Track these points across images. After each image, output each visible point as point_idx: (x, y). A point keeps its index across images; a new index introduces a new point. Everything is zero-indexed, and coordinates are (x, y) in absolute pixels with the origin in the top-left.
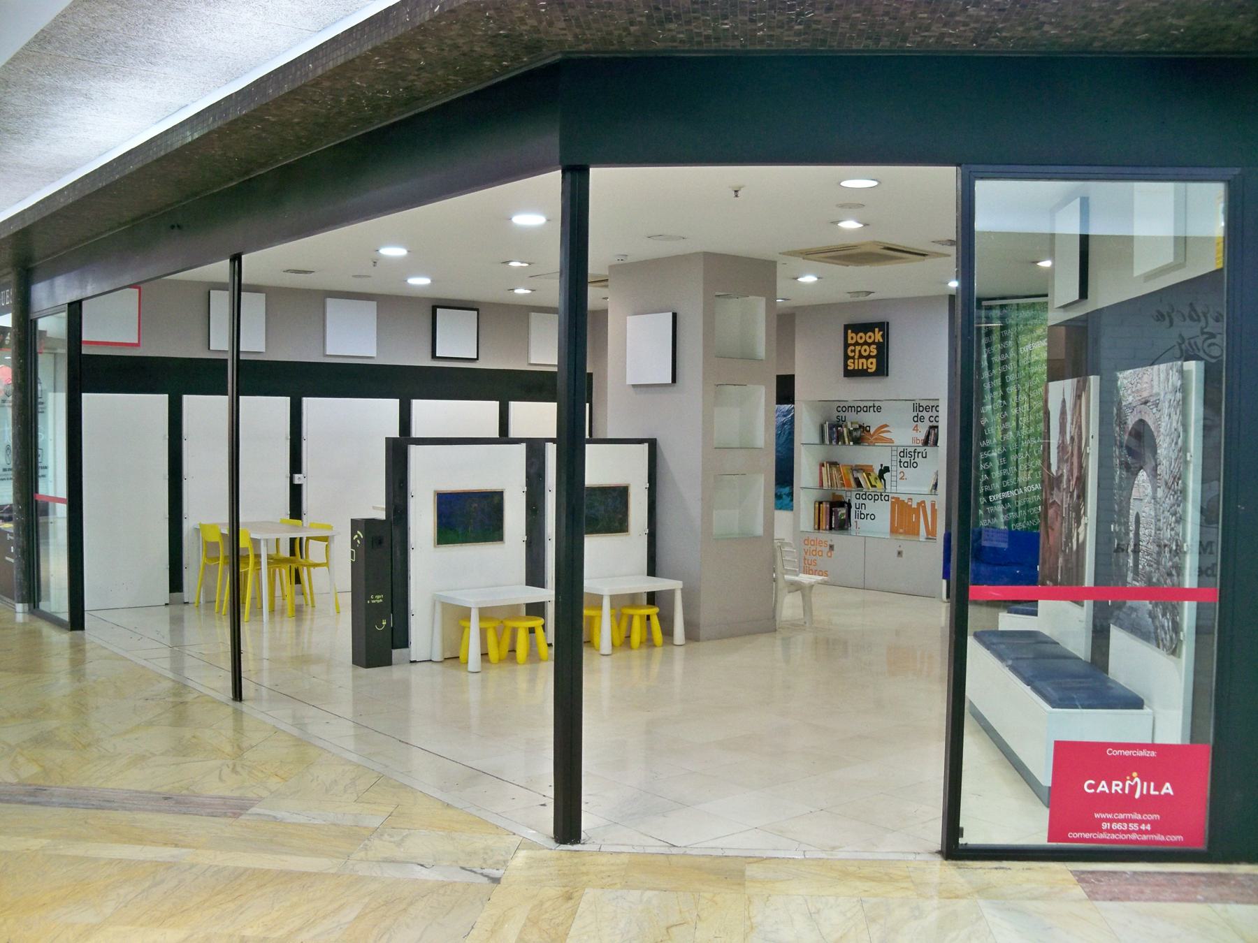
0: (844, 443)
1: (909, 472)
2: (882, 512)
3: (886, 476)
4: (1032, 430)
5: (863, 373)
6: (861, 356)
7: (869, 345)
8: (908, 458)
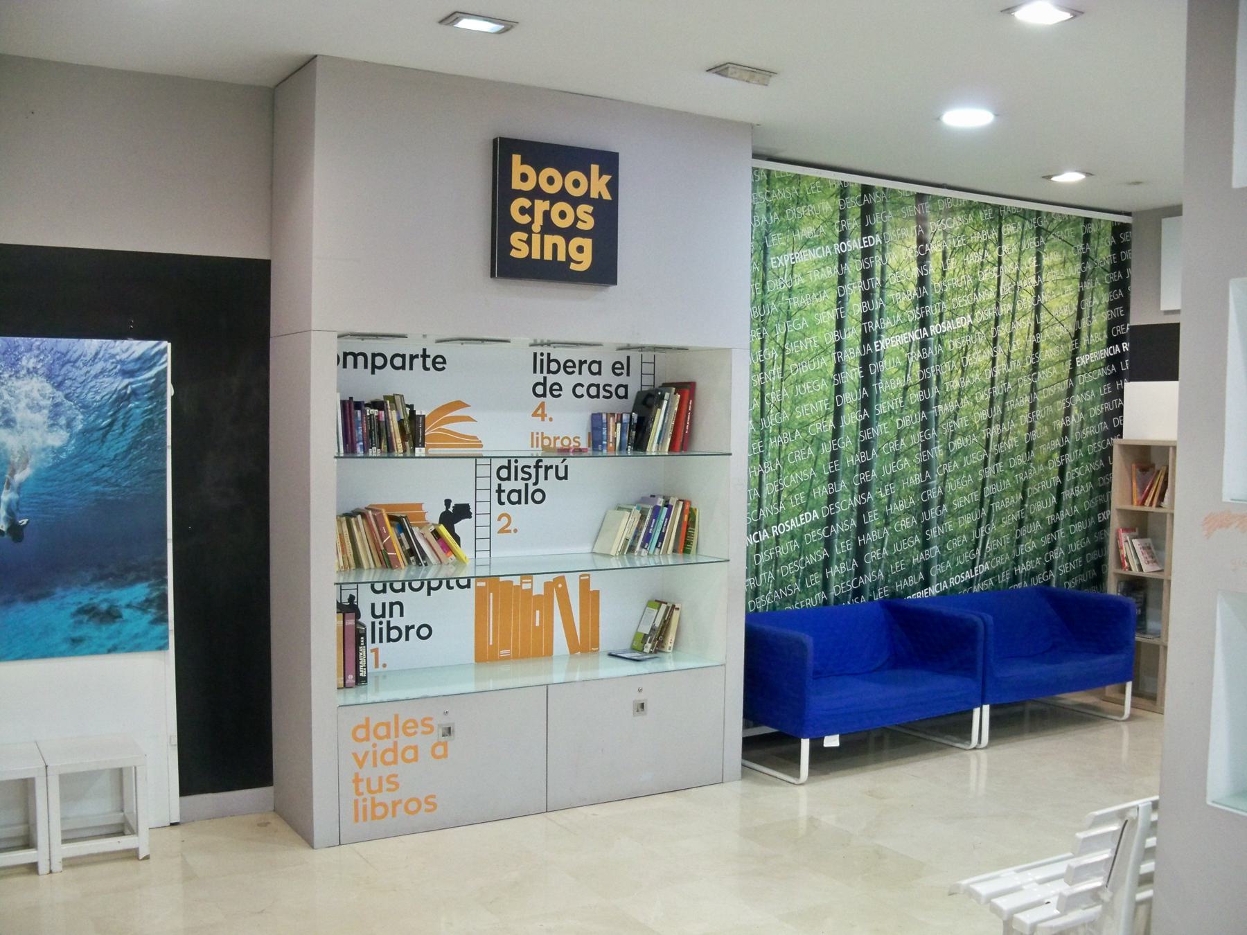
0: (390, 448)
1: (523, 514)
2: (452, 617)
3: (461, 527)
4: (785, 416)
5: (553, 272)
6: (549, 227)
7: (575, 202)
8: (523, 480)
